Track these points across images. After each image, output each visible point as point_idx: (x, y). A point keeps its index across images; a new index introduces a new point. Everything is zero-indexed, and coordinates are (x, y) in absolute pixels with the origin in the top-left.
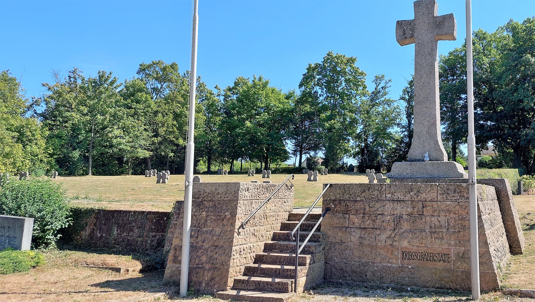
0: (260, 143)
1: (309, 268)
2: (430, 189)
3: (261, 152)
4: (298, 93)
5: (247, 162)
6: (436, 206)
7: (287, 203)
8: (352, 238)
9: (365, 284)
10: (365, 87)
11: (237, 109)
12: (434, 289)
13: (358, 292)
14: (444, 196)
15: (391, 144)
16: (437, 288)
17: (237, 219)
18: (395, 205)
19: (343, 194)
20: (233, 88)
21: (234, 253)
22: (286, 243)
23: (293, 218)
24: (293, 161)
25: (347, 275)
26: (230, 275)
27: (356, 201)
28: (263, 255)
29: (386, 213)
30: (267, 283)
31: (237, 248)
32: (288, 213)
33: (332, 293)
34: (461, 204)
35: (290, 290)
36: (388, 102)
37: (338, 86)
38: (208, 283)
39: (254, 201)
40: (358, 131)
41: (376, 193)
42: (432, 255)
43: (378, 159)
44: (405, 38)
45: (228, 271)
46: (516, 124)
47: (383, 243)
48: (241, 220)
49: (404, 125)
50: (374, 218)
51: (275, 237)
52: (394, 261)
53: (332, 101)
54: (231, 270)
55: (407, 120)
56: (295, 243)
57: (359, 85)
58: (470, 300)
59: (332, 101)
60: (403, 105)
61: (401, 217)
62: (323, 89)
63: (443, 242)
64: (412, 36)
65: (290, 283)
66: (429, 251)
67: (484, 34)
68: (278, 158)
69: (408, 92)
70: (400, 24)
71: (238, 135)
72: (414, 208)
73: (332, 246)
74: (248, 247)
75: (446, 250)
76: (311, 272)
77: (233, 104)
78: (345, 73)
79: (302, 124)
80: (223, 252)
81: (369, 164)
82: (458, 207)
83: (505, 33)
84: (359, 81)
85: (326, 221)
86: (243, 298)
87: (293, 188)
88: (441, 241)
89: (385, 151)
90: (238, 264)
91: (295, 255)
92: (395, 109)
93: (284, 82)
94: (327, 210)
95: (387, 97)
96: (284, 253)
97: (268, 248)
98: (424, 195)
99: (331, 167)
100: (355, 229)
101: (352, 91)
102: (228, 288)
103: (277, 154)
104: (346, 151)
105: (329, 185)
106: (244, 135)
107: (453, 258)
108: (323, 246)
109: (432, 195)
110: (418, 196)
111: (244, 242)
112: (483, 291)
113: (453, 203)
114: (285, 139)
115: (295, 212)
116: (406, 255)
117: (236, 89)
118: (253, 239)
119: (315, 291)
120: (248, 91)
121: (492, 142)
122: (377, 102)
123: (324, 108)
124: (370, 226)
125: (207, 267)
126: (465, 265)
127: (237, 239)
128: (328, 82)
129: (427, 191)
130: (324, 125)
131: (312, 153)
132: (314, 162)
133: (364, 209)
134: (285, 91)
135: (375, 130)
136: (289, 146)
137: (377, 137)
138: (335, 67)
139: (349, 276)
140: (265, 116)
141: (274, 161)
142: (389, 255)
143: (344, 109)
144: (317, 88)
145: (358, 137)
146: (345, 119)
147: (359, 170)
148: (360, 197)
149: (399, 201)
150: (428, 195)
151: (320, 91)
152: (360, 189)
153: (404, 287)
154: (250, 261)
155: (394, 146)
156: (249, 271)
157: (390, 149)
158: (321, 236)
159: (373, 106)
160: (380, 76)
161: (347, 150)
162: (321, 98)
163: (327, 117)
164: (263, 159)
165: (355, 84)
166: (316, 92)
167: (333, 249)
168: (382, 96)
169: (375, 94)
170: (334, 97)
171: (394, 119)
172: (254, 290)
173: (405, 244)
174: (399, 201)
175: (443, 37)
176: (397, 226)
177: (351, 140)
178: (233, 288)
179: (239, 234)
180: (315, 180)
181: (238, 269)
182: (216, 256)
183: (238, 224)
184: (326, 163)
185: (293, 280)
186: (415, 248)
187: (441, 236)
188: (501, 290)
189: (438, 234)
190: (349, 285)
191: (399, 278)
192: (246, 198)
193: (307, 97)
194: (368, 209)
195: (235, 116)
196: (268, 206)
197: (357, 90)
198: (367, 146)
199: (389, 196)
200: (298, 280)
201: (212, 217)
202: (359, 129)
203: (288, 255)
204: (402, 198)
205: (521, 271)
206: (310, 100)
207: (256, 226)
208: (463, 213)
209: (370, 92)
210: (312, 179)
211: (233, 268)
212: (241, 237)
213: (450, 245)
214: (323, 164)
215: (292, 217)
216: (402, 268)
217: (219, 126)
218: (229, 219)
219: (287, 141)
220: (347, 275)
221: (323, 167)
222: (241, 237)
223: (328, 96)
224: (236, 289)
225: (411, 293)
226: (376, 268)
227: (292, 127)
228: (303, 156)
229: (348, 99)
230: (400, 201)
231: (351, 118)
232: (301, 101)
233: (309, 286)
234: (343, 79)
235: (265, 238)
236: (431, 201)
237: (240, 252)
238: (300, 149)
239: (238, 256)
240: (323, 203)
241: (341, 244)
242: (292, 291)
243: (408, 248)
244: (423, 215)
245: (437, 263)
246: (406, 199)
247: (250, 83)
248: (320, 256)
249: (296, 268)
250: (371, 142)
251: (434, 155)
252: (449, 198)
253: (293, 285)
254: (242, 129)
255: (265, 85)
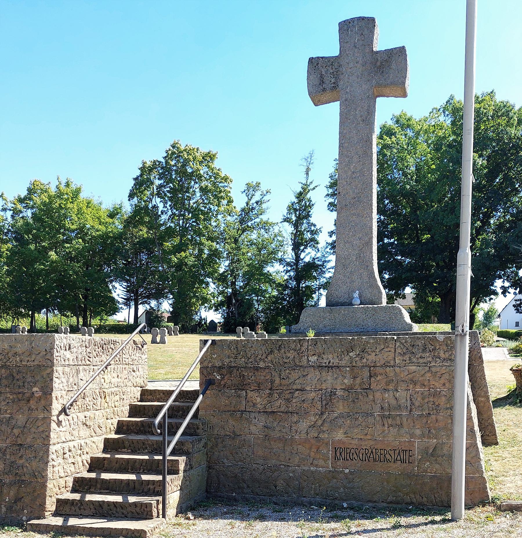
0: (73, 286)
1: (184, 477)
2: (382, 347)
3: (76, 300)
4: (128, 208)
5: (55, 316)
6: (392, 374)
7: (137, 373)
8: (253, 428)
9: (274, 499)
10: (230, 201)
11: (35, 231)
12: (385, 505)
13: (265, 511)
14: (407, 357)
15: (270, 290)
16: (391, 502)
17: (54, 398)
18: (324, 374)
19: (236, 358)
20: (25, 198)
21: (51, 456)
22: (141, 437)
23: (149, 397)
24: (125, 315)
25: (245, 485)
26: (48, 493)
27: (257, 369)
28: (104, 459)
29: (308, 388)
30: (115, 504)
31: (58, 447)
32: (140, 389)
33: (223, 516)
34: (433, 369)
35: (155, 514)
36: (266, 226)
37: (189, 199)
38: (11, 507)
39: (81, 368)
40: (221, 270)
41: (291, 354)
42: (382, 452)
43: (252, 313)
44: (324, 90)
45: (44, 486)
46: (447, 261)
47: (303, 436)
48: (61, 401)
49: (288, 260)
50: (289, 396)
51: (121, 428)
52: (321, 462)
53: (181, 222)
54: (50, 485)
55: (293, 254)
56: (161, 438)
57: (221, 197)
58: (449, 521)
59: (181, 222)
60: (288, 229)
61: (333, 393)
62: (166, 203)
63: (402, 431)
64: (335, 87)
65: (154, 503)
66: (379, 446)
67: (409, 120)
68: (102, 310)
69: (295, 210)
70: (314, 63)
71: (39, 274)
72: (355, 378)
73: (219, 441)
74: (76, 445)
75: (407, 444)
76: (188, 483)
77: (27, 224)
78: (200, 177)
79: (136, 258)
80: (33, 455)
81: (239, 320)
82: (428, 375)
83: (442, 118)
84: (220, 192)
85: (208, 402)
86: (75, 530)
87: (145, 346)
88: (398, 430)
89: (262, 302)
90: (62, 475)
91: (161, 458)
92: (276, 236)
93: (106, 189)
94: (207, 383)
95: (264, 217)
96: (139, 454)
97: (110, 446)
98: (372, 357)
99: (183, 325)
100: (257, 415)
101: (212, 206)
102: (46, 514)
103: (100, 305)
104: (205, 300)
105: (210, 342)
106: (48, 273)
107: (417, 456)
108: (203, 441)
109: (387, 356)
110: (362, 358)
111: (69, 438)
112: (468, 507)
113: (421, 368)
114: (111, 282)
115: (150, 387)
116: (341, 452)
117: (30, 199)
118: (84, 432)
119: (195, 513)
120: (51, 203)
121: (412, 288)
122: (249, 224)
123: (170, 233)
124: (282, 409)
125: (7, 481)
126: (437, 466)
127: (57, 434)
128: (173, 191)
129: (377, 350)
130: (170, 259)
131: (153, 303)
132: (157, 317)
133: (272, 382)
134: (107, 205)
135: (246, 269)
136: (118, 291)
137: (249, 280)
138: (184, 166)
139: (248, 487)
140: (79, 244)
141: (96, 314)
142: (312, 454)
143: (200, 234)
144: (157, 201)
145: (222, 279)
146: (201, 251)
147: (224, 329)
148: (264, 362)
149: (329, 367)
150: (380, 356)
151: (161, 206)
152: (264, 348)
153: (337, 502)
154: (82, 468)
155: (275, 293)
156: (80, 485)
157: (269, 297)
158: (201, 426)
159: (244, 231)
160: (254, 184)
161: (206, 298)
162: (164, 217)
163: (174, 247)
164: (80, 311)
165: (216, 196)
166: (155, 207)
167: (220, 445)
168: (257, 216)
169: (247, 212)
170: (184, 215)
171: (274, 252)
172: (93, 516)
173: (339, 435)
174: (329, 367)
175: (387, 91)
176: (326, 408)
177: (211, 284)
178: (56, 514)
179: (59, 424)
180: (163, 342)
181: (62, 482)
182: (21, 462)
183: (56, 407)
184: (174, 317)
185: (160, 498)
186: (355, 442)
187: (398, 422)
188: (493, 502)
189: (394, 419)
190: (247, 500)
191: (329, 489)
192: (67, 363)
193: (142, 215)
194: (277, 381)
195: (32, 243)
196: (105, 377)
197: (218, 205)
198: (235, 293)
199: (313, 359)
200: (167, 497)
201: (9, 395)
202: (223, 266)
203: (147, 457)
204: (335, 361)
205: (512, 472)
206: (147, 219)
207: (88, 410)
208: (437, 384)
209: (238, 209)
210: (158, 340)
211: (54, 481)
212: (64, 429)
213: (412, 435)
214: (170, 320)
215: (146, 394)
216: (334, 474)
217: (7, 258)
218: (40, 398)
219: (114, 283)
220: (245, 485)
221: (171, 325)
222: (64, 429)
223: (174, 214)
224: (60, 515)
225: (351, 513)
226: (291, 475)
227: (121, 263)
228: (140, 307)
229: (204, 220)
230: (332, 367)
231: (210, 250)
232: (134, 220)
233: (184, 506)
234: (197, 186)
235: (104, 429)
236: (385, 365)
237: (64, 454)
238: (134, 297)
239: (60, 460)
240: (201, 373)
241: (233, 438)
242: (158, 517)
243: (344, 443)
244: (370, 388)
245: (391, 464)
246: (343, 363)
247: (53, 190)
248: (199, 457)
249: (164, 478)
250: (241, 287)
251: (368, 295)
252: (414, 360)
253: (160, 506)
254: (44, 264)
255: (77, 192)
